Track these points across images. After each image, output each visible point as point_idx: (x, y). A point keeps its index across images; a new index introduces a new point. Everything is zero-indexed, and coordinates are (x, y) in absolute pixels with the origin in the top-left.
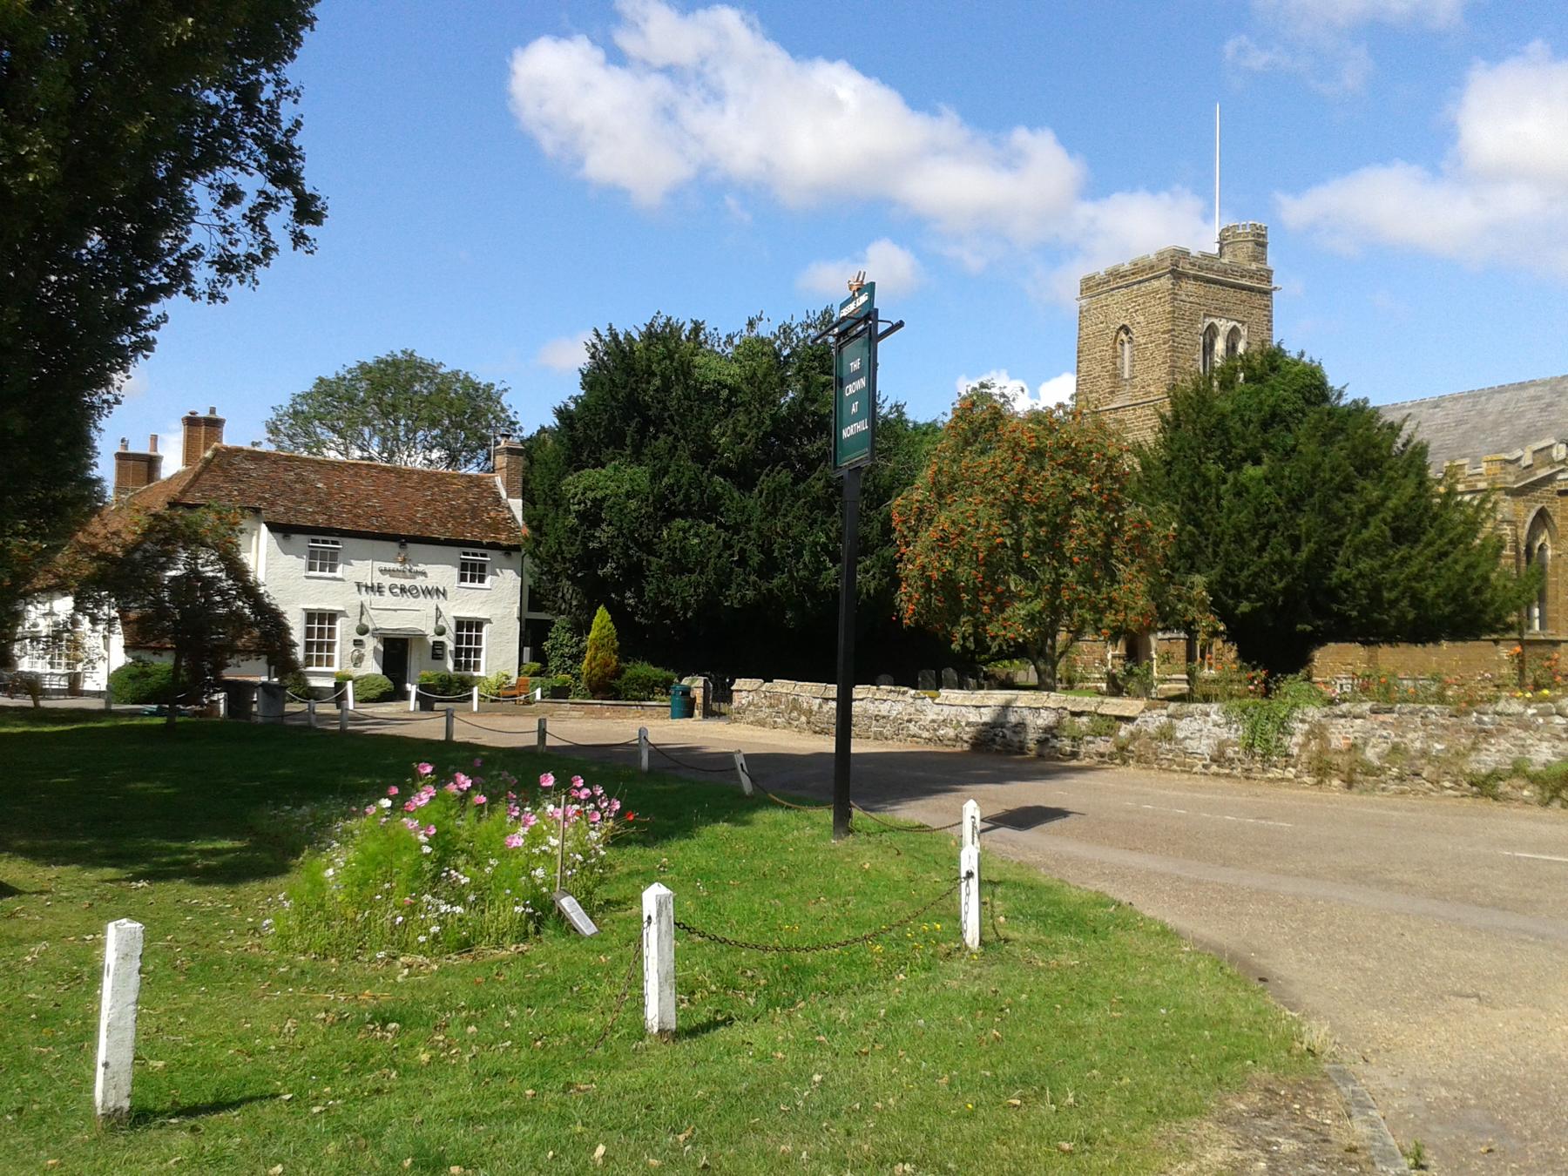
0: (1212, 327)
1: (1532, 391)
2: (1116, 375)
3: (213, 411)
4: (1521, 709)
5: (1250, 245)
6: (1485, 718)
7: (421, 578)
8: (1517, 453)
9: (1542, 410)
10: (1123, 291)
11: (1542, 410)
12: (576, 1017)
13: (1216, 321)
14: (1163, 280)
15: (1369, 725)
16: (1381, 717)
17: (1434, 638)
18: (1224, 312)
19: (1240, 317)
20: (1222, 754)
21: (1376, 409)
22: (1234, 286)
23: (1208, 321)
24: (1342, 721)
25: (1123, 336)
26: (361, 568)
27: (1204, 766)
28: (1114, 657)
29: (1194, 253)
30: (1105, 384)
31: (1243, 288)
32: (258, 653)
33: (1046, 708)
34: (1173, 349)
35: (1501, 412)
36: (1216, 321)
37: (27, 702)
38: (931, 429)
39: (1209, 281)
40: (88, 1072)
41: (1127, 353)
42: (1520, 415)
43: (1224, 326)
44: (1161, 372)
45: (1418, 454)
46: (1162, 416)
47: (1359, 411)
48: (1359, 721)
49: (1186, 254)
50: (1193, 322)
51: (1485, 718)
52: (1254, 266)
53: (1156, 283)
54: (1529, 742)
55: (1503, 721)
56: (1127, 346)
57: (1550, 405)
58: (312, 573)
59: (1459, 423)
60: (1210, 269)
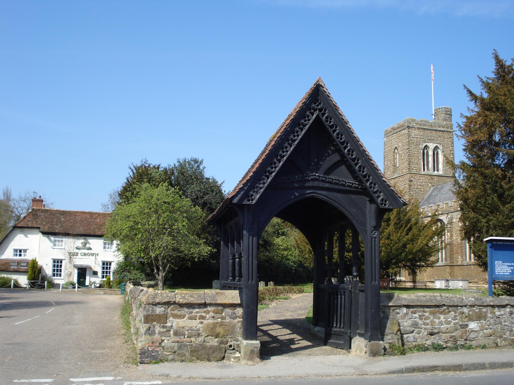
0: (426, 147)
2: (395, 166)
3: (40, 197)
5: (443, 115)
7: (374, 223)
10: (396, 134)
12: (91, 351)
14: (406, 130)
18: (431, 141)
19: (439, 142)
22: (436, 130)
23: (424, 144)
25: (396, 151)
26: (70, 244)
31: (440, 131)
34: (409, 156)
36: (428, 144)
37: (237, 275)
39: (424, 129)
40: (81, 376)
43: (432, 146)
49: (414, 120)
50: (418, 144)
52: (445, 123)
53: (404, 131)
58: (54, 247)
60: (425, 125)
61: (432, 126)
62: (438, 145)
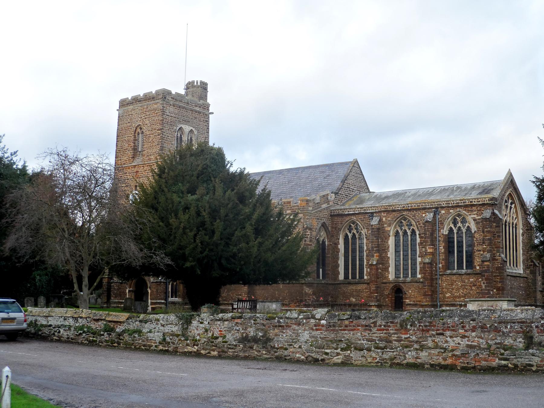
1: (321, 169)
2: (135, 149)
4: (296, 316)
6: (281, 321)
8: (313, 197)
9: (325, 178)
11: (325, 178)
13: (183, 126)
15: (230, 325)
16: (236, 321)
17: (275, 282)
18: (187, 122)
20: (164, 339)
21: (248, 174)
23: (179, 126)
24: (219, 323)
27: (156, 346)
28: (129, 291)
29: (173, 93)
30: (130, 153)
32: (37, 298)
33: (81, 318)
34: (162, 138)
35: (307, 178)
36: (183, 126)
38: (28, 174)
41: (140, 140)
42: (316, 179)
44: (157, 149)
45: (266, 196)
46: (152, 171)
47: (241, 176)
48: (226, 323)
51: (281, 321)
54: (300, 331)
55: (289, 321)
56: (140, 135)
57: (328, 176)
59: (289, 182)
61: (188, 103)
62: (194, 129)
